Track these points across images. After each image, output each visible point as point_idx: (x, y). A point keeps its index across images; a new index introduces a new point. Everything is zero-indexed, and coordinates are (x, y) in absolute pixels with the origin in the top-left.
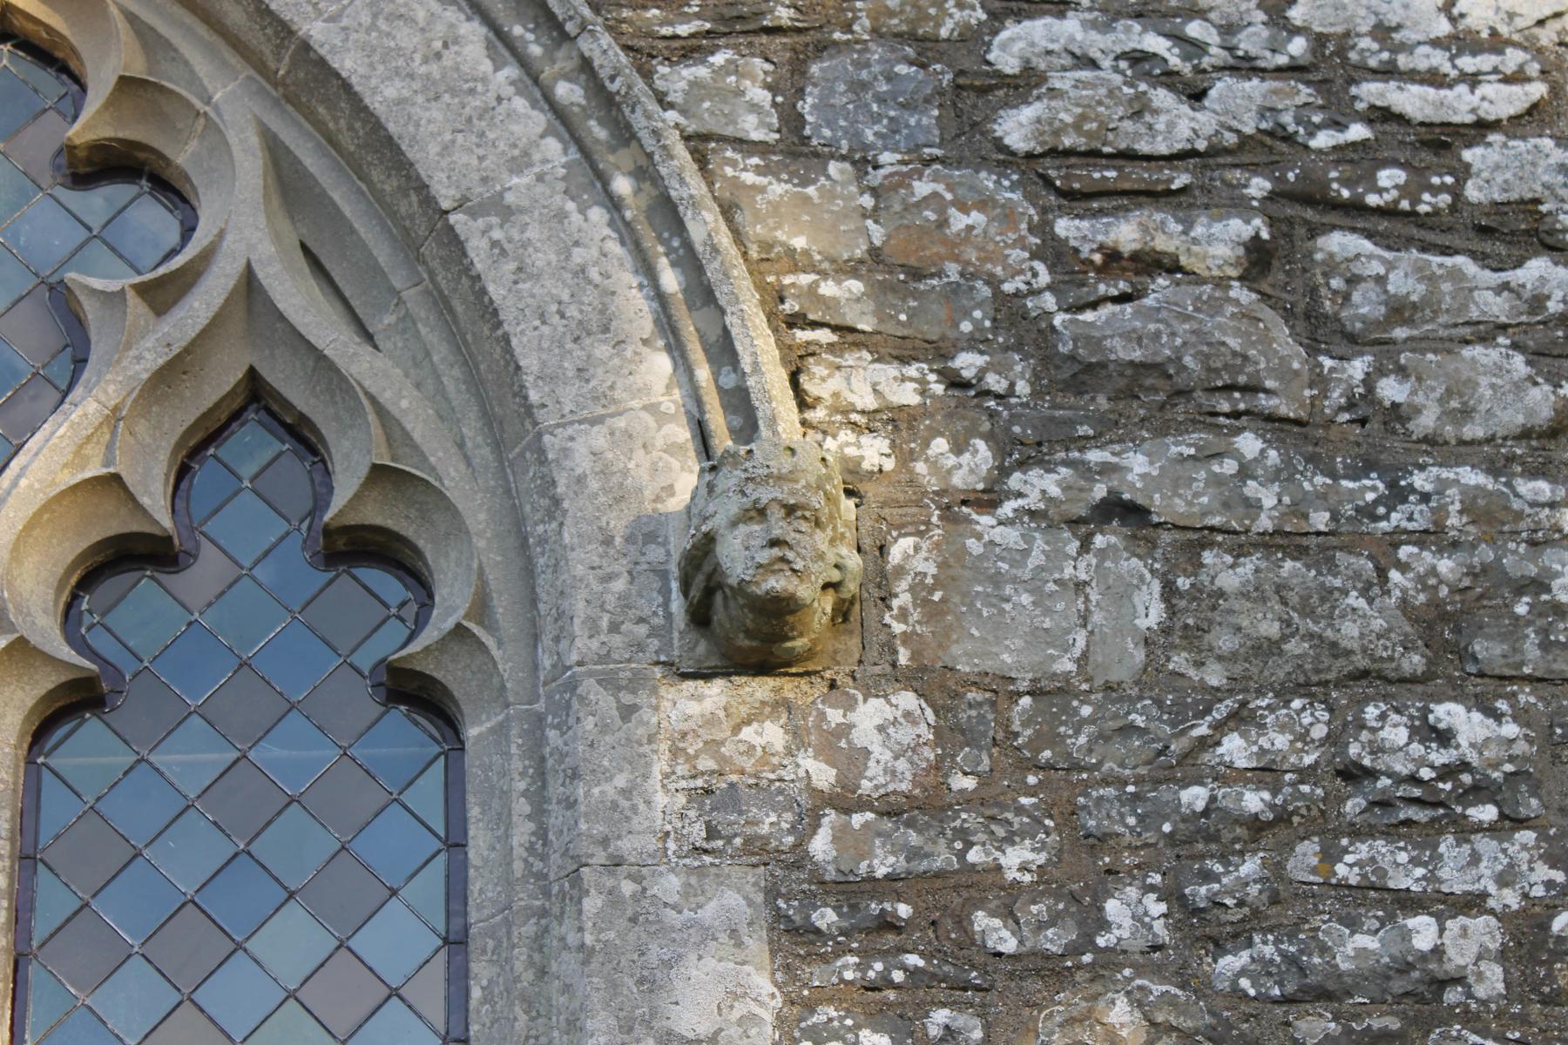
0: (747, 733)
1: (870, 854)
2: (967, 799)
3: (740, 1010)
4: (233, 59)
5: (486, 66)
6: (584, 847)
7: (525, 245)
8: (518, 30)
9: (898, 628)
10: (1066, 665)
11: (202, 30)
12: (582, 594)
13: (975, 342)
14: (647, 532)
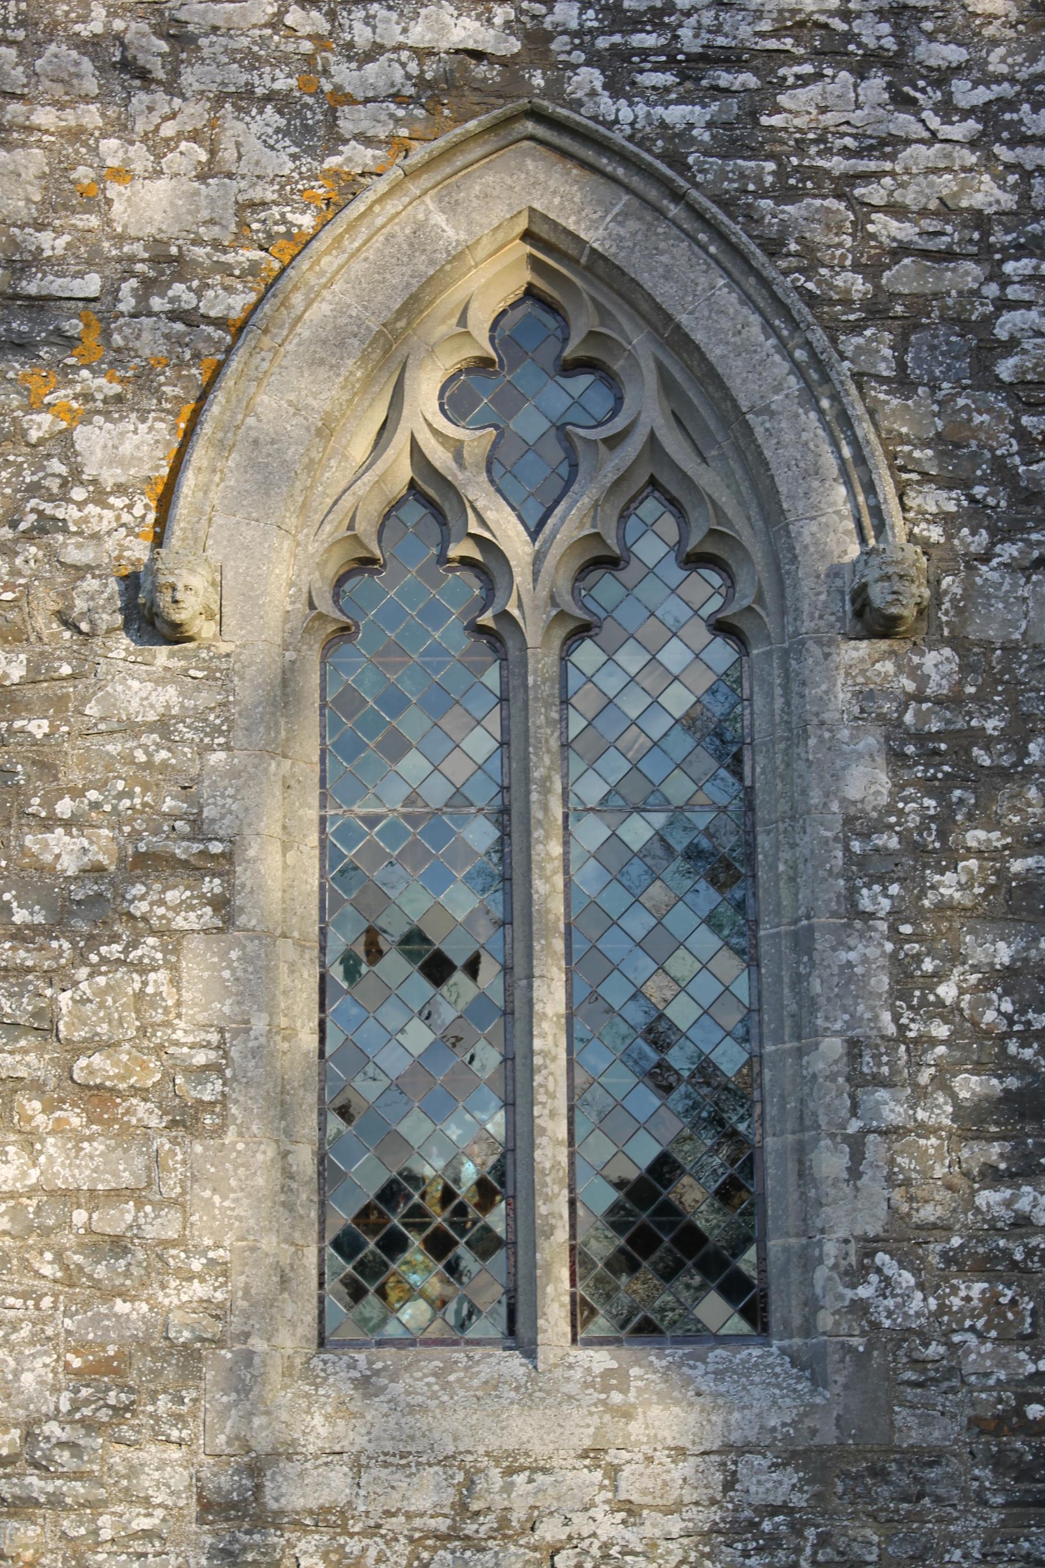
0: (878, 666)
1: (929, 722)
2: (972, 698)
3: (873, 789)
4: (641, 322)
5: (762, 338)
6: (809, 717)
7: (781, 430)
8: (777, 322)
9: (944, 619)
10: (1017, 636)
11: (626, 307)
12: (807, 601)
13: (982, 481)
14: (835, 572)
